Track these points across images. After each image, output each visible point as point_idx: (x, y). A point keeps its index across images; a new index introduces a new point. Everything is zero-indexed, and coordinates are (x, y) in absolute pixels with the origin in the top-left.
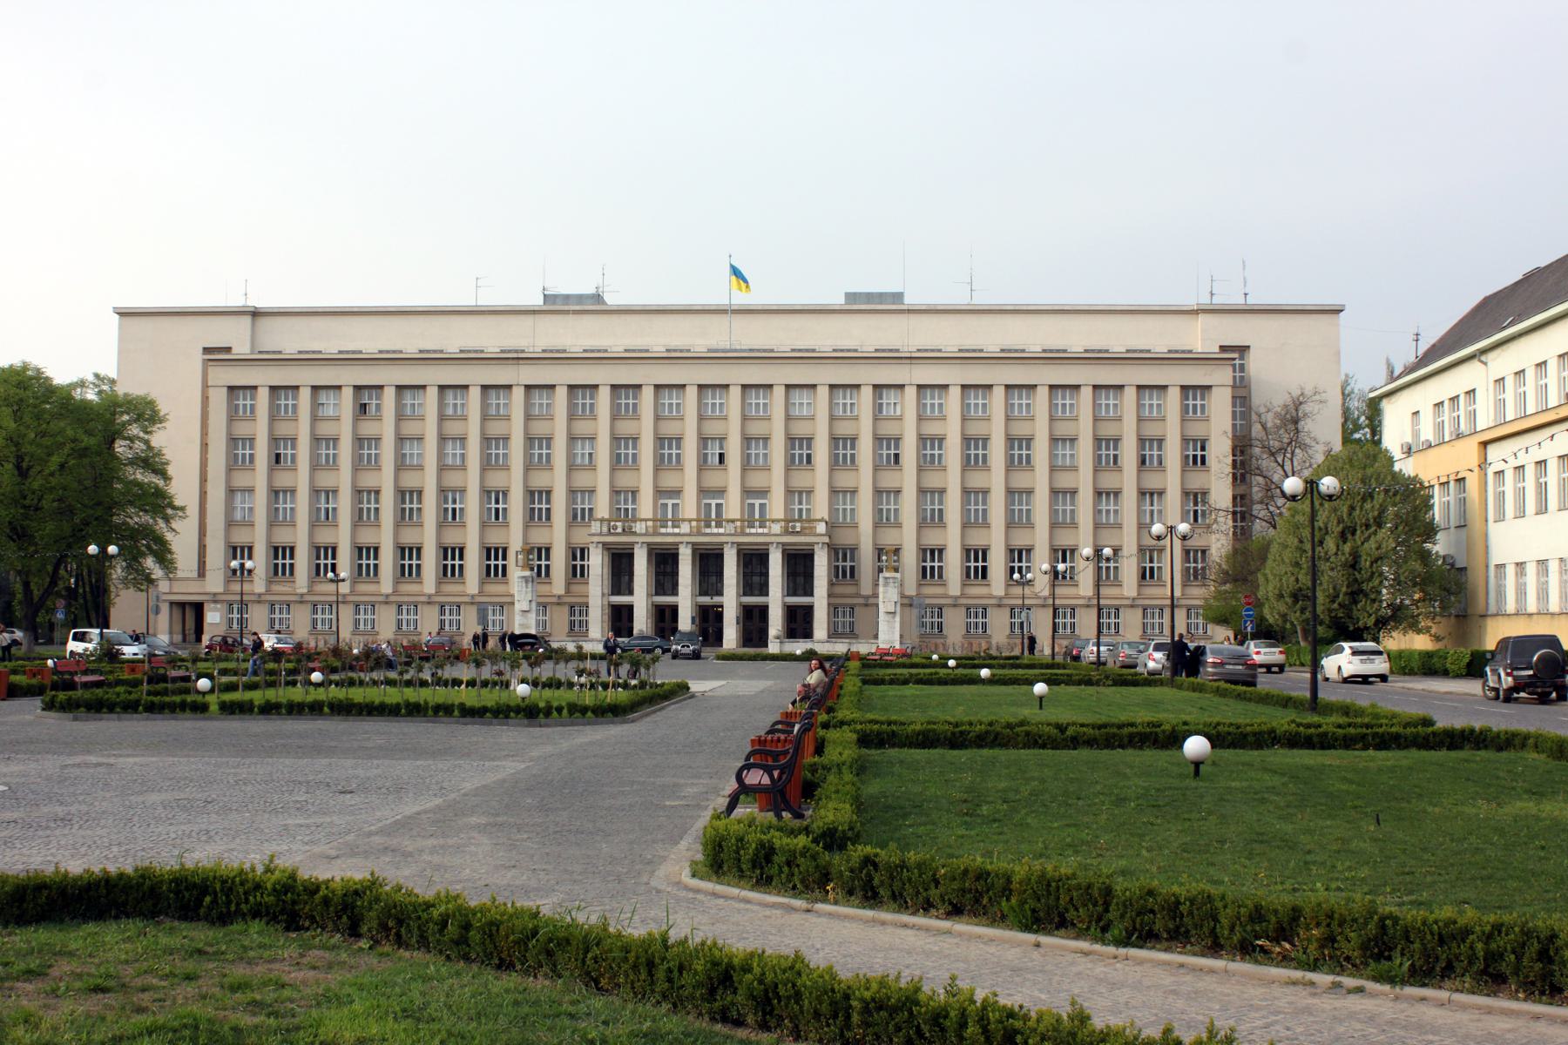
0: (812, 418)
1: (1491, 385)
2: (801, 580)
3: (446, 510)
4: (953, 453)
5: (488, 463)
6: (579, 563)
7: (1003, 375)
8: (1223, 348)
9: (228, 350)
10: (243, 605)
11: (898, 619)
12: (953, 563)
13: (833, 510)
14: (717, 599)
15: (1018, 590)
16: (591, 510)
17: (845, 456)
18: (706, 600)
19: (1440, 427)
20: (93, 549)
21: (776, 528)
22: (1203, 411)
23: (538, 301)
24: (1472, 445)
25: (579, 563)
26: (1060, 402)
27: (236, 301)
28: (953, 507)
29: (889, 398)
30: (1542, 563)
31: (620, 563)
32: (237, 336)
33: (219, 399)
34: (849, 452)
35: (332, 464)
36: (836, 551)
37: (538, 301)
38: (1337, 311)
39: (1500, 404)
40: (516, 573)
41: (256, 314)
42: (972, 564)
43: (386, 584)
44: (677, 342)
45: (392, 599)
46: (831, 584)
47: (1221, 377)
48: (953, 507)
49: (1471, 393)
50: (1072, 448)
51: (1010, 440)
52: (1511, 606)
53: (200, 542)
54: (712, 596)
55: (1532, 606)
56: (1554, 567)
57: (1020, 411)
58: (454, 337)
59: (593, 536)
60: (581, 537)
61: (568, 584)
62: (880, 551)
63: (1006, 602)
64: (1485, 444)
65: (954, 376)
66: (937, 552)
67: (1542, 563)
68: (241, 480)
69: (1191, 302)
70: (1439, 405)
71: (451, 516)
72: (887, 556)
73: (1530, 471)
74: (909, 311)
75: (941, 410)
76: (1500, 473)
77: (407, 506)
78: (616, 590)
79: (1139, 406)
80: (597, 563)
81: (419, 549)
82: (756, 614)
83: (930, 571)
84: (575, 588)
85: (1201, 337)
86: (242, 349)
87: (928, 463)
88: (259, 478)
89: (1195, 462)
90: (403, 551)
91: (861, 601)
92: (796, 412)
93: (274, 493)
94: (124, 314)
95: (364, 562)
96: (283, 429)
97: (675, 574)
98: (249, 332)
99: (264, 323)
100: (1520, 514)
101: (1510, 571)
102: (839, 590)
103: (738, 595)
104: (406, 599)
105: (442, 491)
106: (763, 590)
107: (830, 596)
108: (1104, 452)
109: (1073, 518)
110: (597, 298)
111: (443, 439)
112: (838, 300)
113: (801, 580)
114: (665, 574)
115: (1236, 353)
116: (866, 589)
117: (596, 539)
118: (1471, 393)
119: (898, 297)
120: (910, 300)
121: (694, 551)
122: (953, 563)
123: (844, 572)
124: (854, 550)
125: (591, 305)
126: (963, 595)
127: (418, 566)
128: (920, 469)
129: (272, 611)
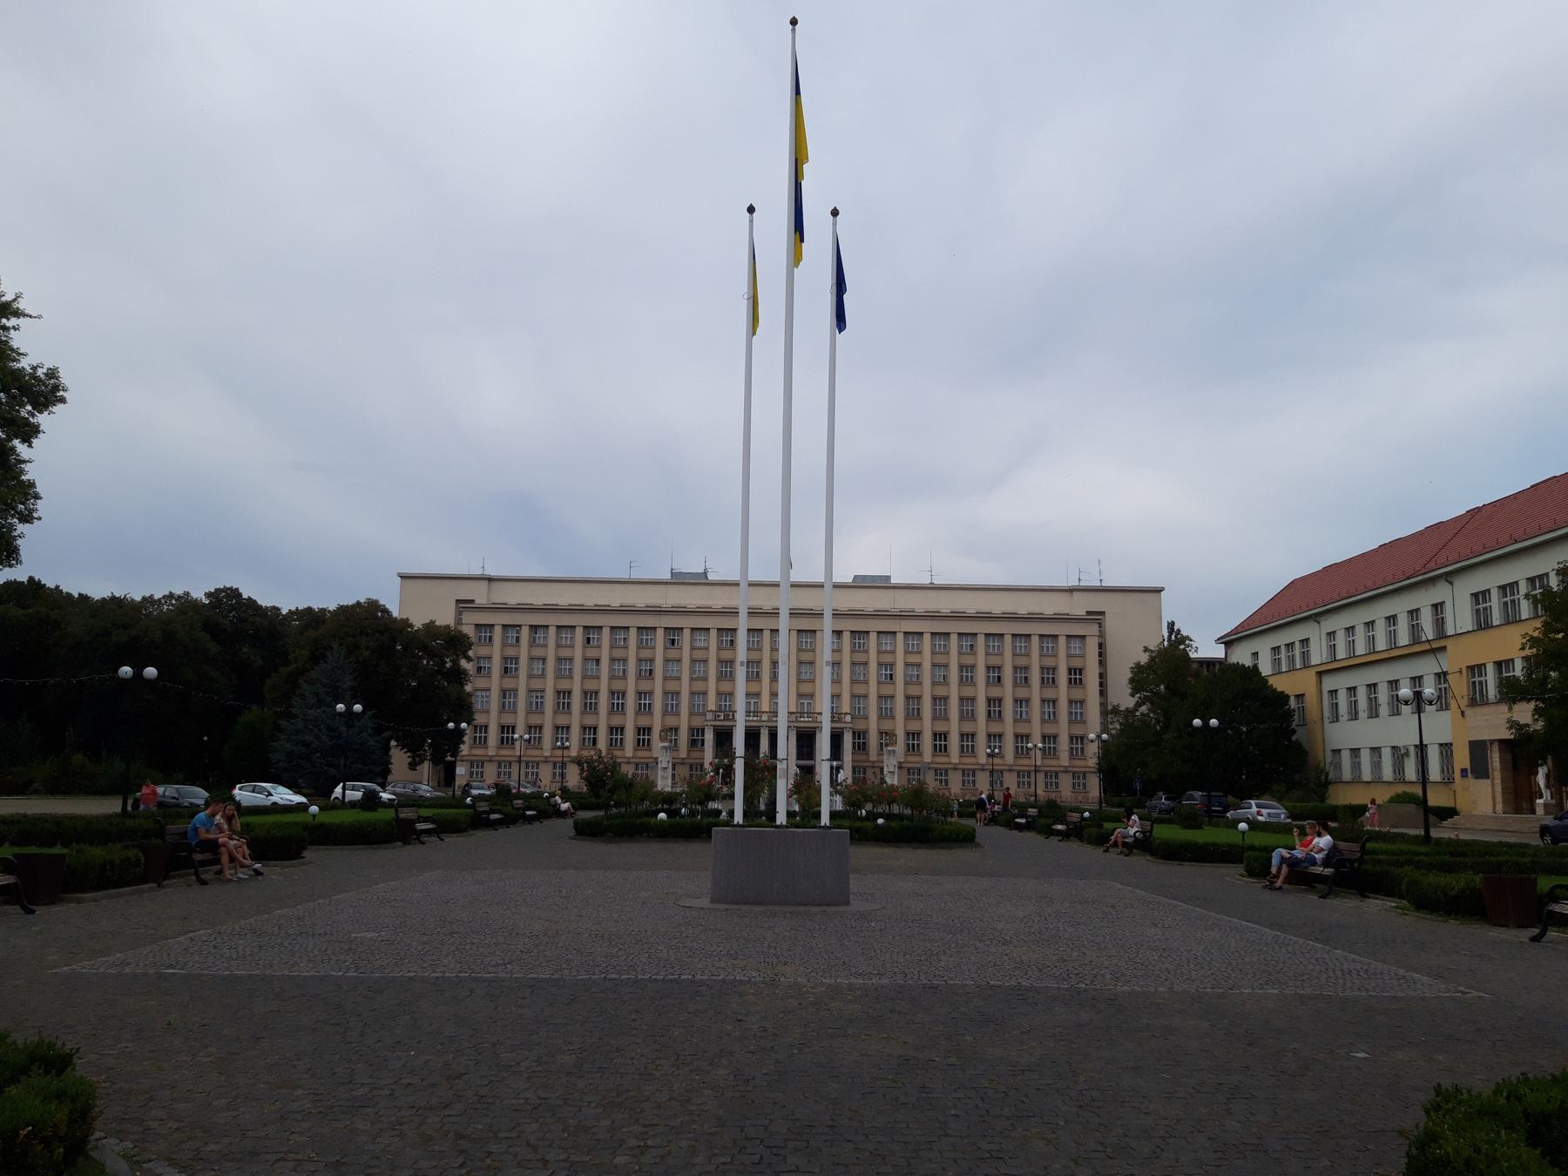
0: (707, 649)
1: (1324, 637)
8: (1089, 613)
9: (472, 601)
10: (563, 765)
12: (954, 742)
15: (559, 752)
18: (809, 763)
21: (765, 717)
23: (667, 576)
24: (1312, 673)
27: (477, 572)
30: (1355, 752)
32: (480, 595)
37: (667, 576)
38: (1159, 591)
40: (658, 744)
41: (490, 579)
43: (1064, 759)
44: (1010, 608)
47: (1092, 629)
52: (1347, 774)
53: (518, 727)
55: (1367, 775)
58: (564, 596)
66: (944, 736)
67: (1376, 750)
69: (1063, 583)
71: (617, 709)
72: (887, 737)
79: (1068, 648)
83: (913, 748)
85: (1079, 606)
86: (480, 601)
94: (403, 577)
99: (496, 585)
100: (1354, 716)
101: (1346, 756)
115: (1096, 617)
116: (873, 757)
125: (700, 580)
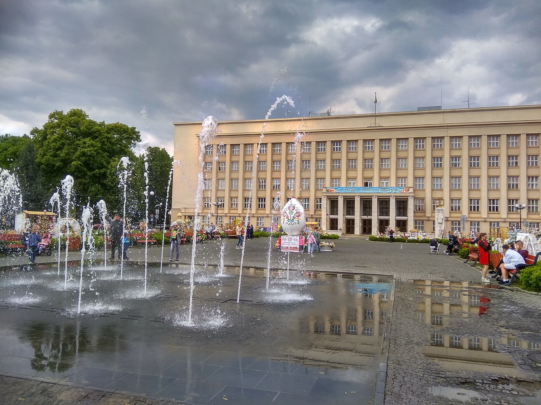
2: (402, 210)
3: (529, 184)
11: (443, 225)
12: (484, 205)
13: (415, 185)
14: (369, 217)
17: (474, 163)
18: (365, 217)
22: (423, 147)
26: (511, 141)
29: (277, 148)
31: (333, 203)
34: (534, 161)
35: (355, 168)
42: (492, 205)
45: (241, 215)
50: (423, 160)
54: (367, 216)
60: (319, 195)
61: (315, 211)
63: (488, 220)
65: (465, 132)
74: (444, 112)
75: (423, 147)
78: (348, 213)
80: (325, 204)
81: (265, 199)
82: (402, 223)
84: (318, 213)
89: (437, 166)
91: (426, 219)
97: (370, 208)
102: (417, 214)
103: (378, 216)
104: (260, 215)
106: (388, 214)
108: (473, 162)
109: (497, 187)
111: (273, 162)
114: (350, 208)
116: (428, 214)
117: (324, 194)
121: (378, 199)
124: (423, 199)
125: (436, 111)
126: (488, 218)
127: (264, 204)
129: (258, 220)
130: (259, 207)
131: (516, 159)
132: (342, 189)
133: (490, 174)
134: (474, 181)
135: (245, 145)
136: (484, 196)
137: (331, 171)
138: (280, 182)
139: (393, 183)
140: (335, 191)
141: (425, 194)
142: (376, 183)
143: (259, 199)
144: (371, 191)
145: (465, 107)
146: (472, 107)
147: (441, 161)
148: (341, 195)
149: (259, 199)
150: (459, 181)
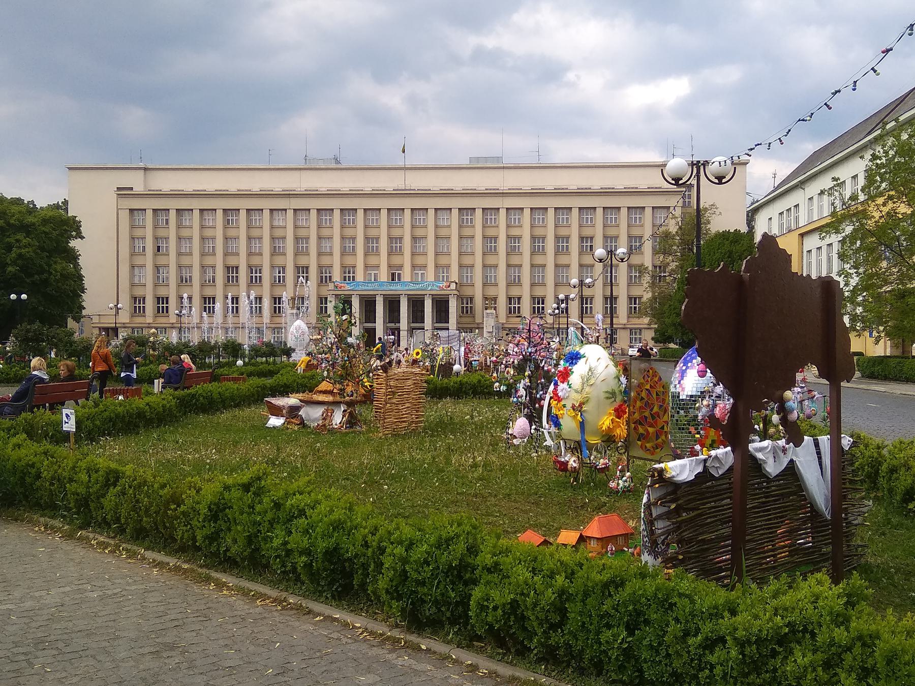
0: (449, 226)
4: (526, 245)
5: (275, 252)
6: (277, 305)
7: (552, 203)
9: (132, 189)
12: (526, 307)
13: (460, 276)
16: (330, 277)
19: (781, 226)
20: (13, 296)
22: (471, 222)
25: (277, 305)
28: (526, 275)
33: (124, 215)
36: (460, 298)
39: (810, 211)
46: (459, 317)
48: (526, 275)
49: (797, 206)
51: (557, 238)
56: (413, 325)
57: (563, 222)
59: (328, 291)
62: (486, 298)
64: (802, 235)
65: (526, 203)
68: (138, 261)
70: (781, 214)
72: (490, 301)
73: (824, 249)
74: (504, 168)
75: (471, 222)
76: (809, 251)
77: (254, 275)
86: (139, 188)
87: (512, 250)
88: (149, 260)
90: (583, 300)
92: (441, 223)
93: (157, 268)
95: (161, 305)
96: (161, 233)
98: (143, 179)
105: (250, 268)
107: (458, 323)
110: (337, 161)
111: (249, 238)
112: (465, 162)
113: (443, 314)
116: (478, 320)
118: (797, 206)
119: (499, 159)
120: (506, 162)
122: (526, 307)
123: (467, 309)
128: (508, 254)
130: (159, 312)
131: (591, 242)
132: (358, 284)
133: (511, 263)
134: (515, 272)
135: (202, 211)
136: (549, 292)
137: (389, 255)
138: (191, 272)
139: (430, 275)
140: (348, 287)
141: (474, 291)
142: (406, 275)
143: (158, 298)
144: (399, 287)
145: (533, 161)
146: (545, 161)
147: (567, 242)
148: (355, 293)
149: (275, 299)
150: (543, 272)
